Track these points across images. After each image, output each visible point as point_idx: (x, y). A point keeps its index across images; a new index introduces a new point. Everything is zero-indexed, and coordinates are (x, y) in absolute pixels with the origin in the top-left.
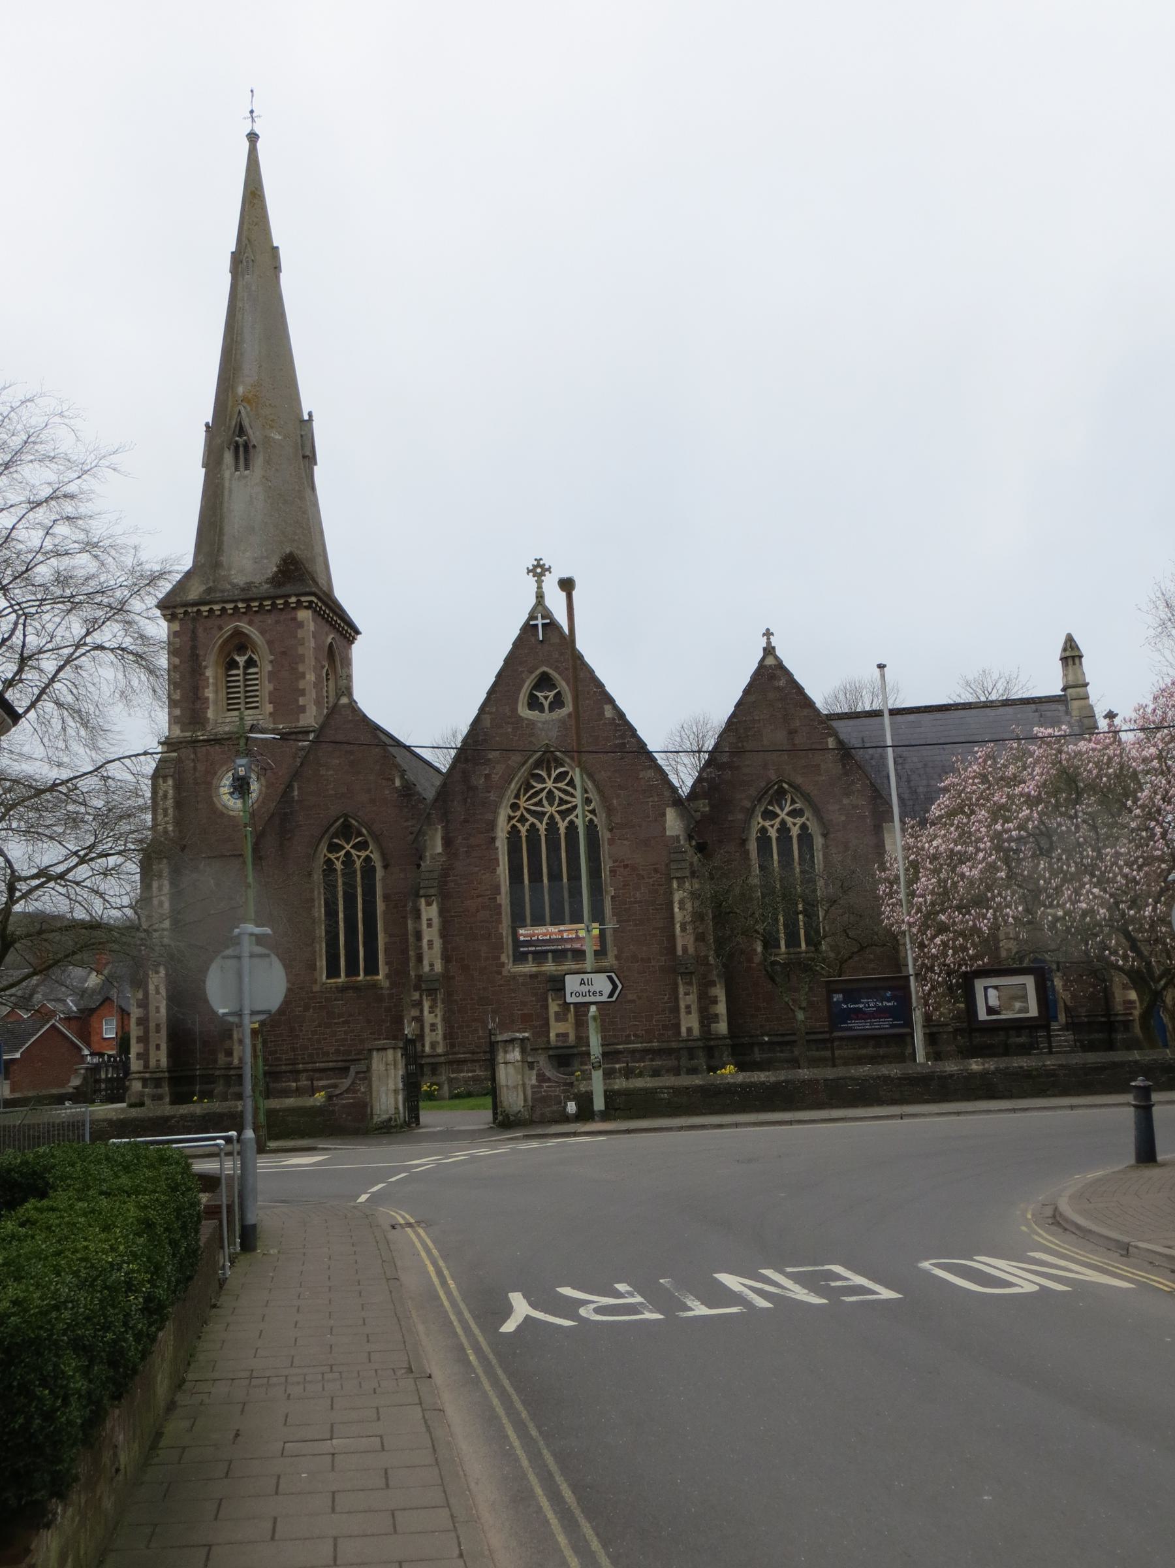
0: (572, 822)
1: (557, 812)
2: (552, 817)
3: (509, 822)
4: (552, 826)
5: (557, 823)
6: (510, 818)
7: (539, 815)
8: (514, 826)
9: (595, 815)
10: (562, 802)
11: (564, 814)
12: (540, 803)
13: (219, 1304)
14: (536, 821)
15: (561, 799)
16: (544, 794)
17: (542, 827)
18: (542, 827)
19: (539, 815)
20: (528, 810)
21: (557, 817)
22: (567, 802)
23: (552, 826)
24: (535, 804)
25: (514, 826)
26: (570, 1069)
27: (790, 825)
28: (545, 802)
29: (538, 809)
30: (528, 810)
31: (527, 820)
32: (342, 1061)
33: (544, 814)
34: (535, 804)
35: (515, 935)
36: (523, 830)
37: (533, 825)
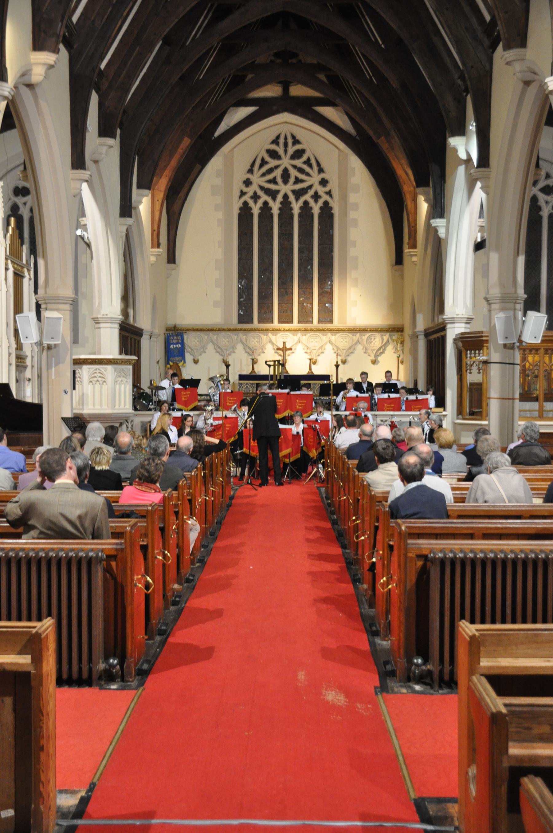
0: (306, 203)
1: (294, 192)
2: (286, 197)
3: (241, 197)
4: (286, 204)
5: (290, 203)
6: (243, 194)
7: (273, 194)
8: (245, 203)
9: (331, 196)
10: (298, 181)
11: (298, 194)
12: (274, 181)
13: (479, 227)
14: (269, 199)
15: (296, 178)
16: (281, 151)
17: (275, 207)
18: (275, 207)
19: (273, 194)
20: (262, 188)
21: (292, 198)
22: (302, 181)
23: (286, 204)
24: (269, 181)
25: (245, 203)
26: (427, 440)
27: (542, 203)
28: (279, 180)
29: (272, 187)
30: (262, 188)
31: (259, 197)
32: (345, 512)
33: (277, 192)
34: (269, 181)
35: (191, 481)
36: (256, 210)
37: (266, 203)
